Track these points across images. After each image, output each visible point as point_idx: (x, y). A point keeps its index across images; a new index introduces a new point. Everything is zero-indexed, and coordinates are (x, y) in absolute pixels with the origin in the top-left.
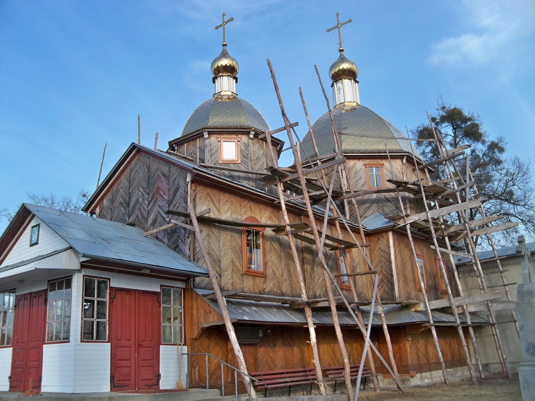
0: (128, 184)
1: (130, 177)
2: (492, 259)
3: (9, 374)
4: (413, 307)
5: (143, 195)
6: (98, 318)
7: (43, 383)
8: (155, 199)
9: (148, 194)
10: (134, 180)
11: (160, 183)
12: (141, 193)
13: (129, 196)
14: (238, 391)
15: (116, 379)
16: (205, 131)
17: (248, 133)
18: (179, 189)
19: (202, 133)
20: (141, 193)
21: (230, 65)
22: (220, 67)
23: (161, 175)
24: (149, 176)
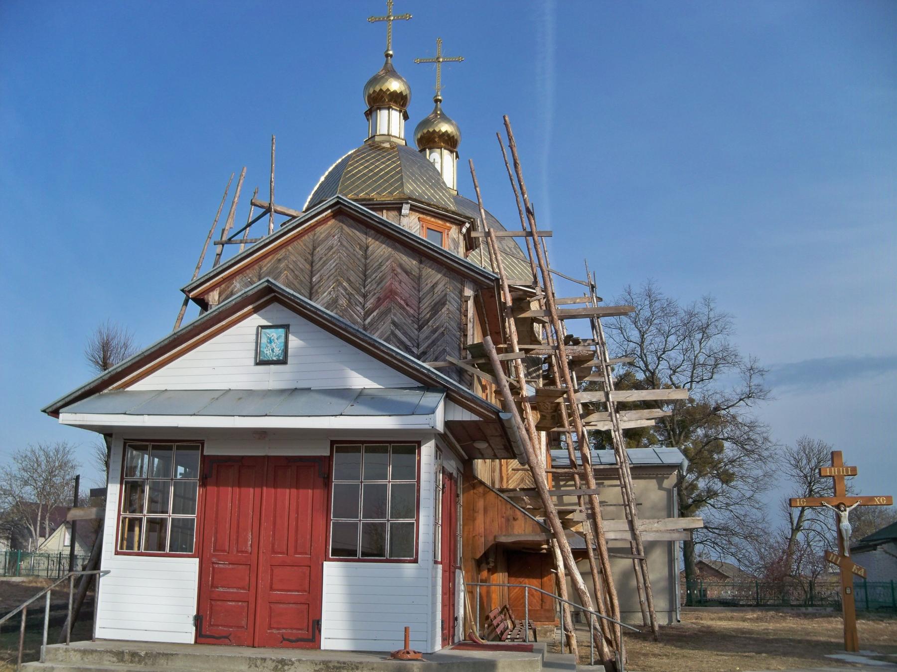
0: (308, 266)
1: (312, 254)
2: (613, 467)
3: (195, 613)
4: (573, 526)
5: (349, 294)
6: (383, 515)
7: (324, 633)
8: (382, 308)
9: (365, 296)
10: (325, 263)
11: (397, 284)
12: (345, 289)
13: (311, 288)
14: (24, 642)
15: (205, 625)
16: (407, 203)
17: (461, 224)
18: (444, 304)
19: (402, 204)
20: (345, 289)
21: (401, 93)
22: (385, 93)
23: (399, 270)
24: (365, 265)
